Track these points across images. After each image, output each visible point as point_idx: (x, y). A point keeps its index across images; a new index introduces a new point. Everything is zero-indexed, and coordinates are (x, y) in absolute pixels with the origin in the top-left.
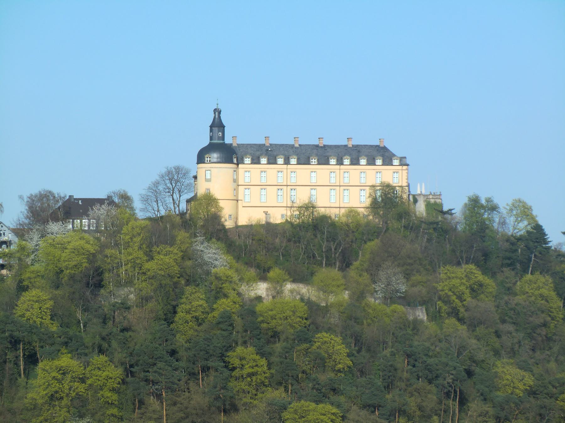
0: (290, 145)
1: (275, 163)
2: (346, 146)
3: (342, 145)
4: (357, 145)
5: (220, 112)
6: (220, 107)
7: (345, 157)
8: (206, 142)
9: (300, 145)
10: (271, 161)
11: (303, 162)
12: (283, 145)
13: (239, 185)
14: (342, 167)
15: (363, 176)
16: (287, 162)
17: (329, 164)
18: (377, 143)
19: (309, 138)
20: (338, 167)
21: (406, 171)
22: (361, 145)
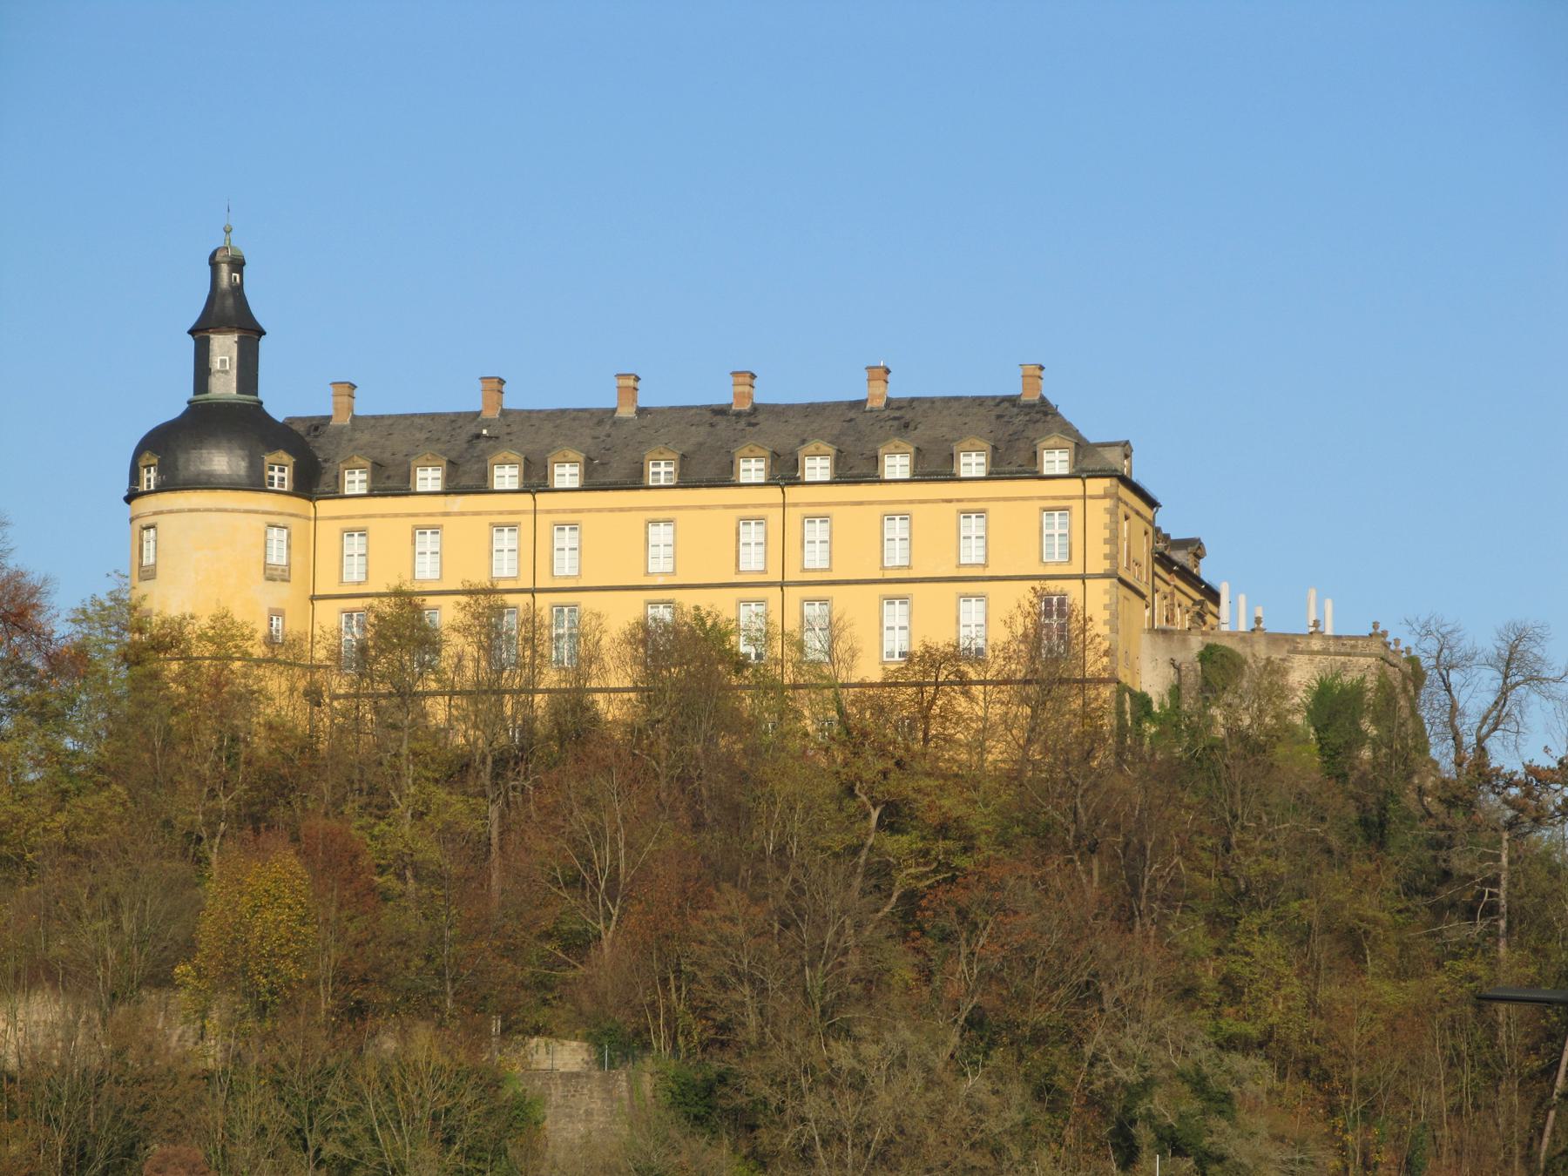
0: (467, 414)
1: (482, 487)
2: (858, 405)
3: (838, 404)
4: (913, 400)
5: (238, 265)
6: (242, 244)
7: (811, 448)
8: (173, 402)
9: (641, 411)
10: (466, 481)
11: (708, 474)
12: (563, 412)
13: (313, 598)
14: (794, 493)
15: (429, 548)
16: (536, 481)
17: (954, 478)
18: (1011, 386)
19: (560, 377)
20: (774, 494)
21: (1108, 503)
22: (932, 401)
